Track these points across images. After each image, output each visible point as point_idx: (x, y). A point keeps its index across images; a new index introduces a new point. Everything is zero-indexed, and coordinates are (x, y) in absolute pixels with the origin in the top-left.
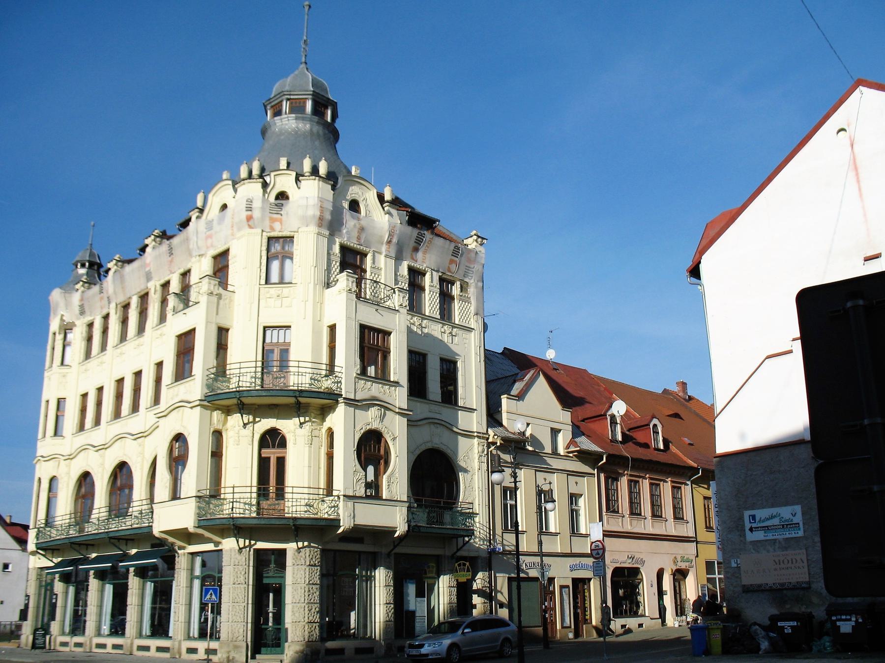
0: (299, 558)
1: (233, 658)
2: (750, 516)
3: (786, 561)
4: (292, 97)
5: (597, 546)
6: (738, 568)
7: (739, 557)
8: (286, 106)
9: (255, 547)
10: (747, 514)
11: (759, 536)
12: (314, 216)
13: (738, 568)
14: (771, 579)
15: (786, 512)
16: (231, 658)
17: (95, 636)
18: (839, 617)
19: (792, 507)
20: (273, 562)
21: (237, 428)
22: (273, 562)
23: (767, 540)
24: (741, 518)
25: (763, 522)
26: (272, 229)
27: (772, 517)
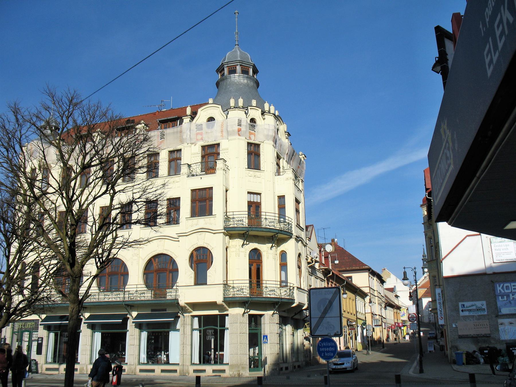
0: (273, 319)
1: (242, 374)
2: (462, 305)
3: (479, 325)
4: (243, 64)
5: (413, 316)
6: (456, 327)
7: (457, 323)
8: (238, 68)
9: (249, 313)
10: (460, 304)
11: (466, 313)
12: (272, 135)
13: (456, 327)
14: (472, 332)
15: (479, 304)
16: (241, 374)
17: (89, 364)
18: (513, 348)
19: (482, 302)
20: (253, 321)
21: (238, 247)
22: (253, 321)
23: (470, 316)
24: (458, 306)
25: (468, 307)
26: (250, 138)
27: (472, 306)
